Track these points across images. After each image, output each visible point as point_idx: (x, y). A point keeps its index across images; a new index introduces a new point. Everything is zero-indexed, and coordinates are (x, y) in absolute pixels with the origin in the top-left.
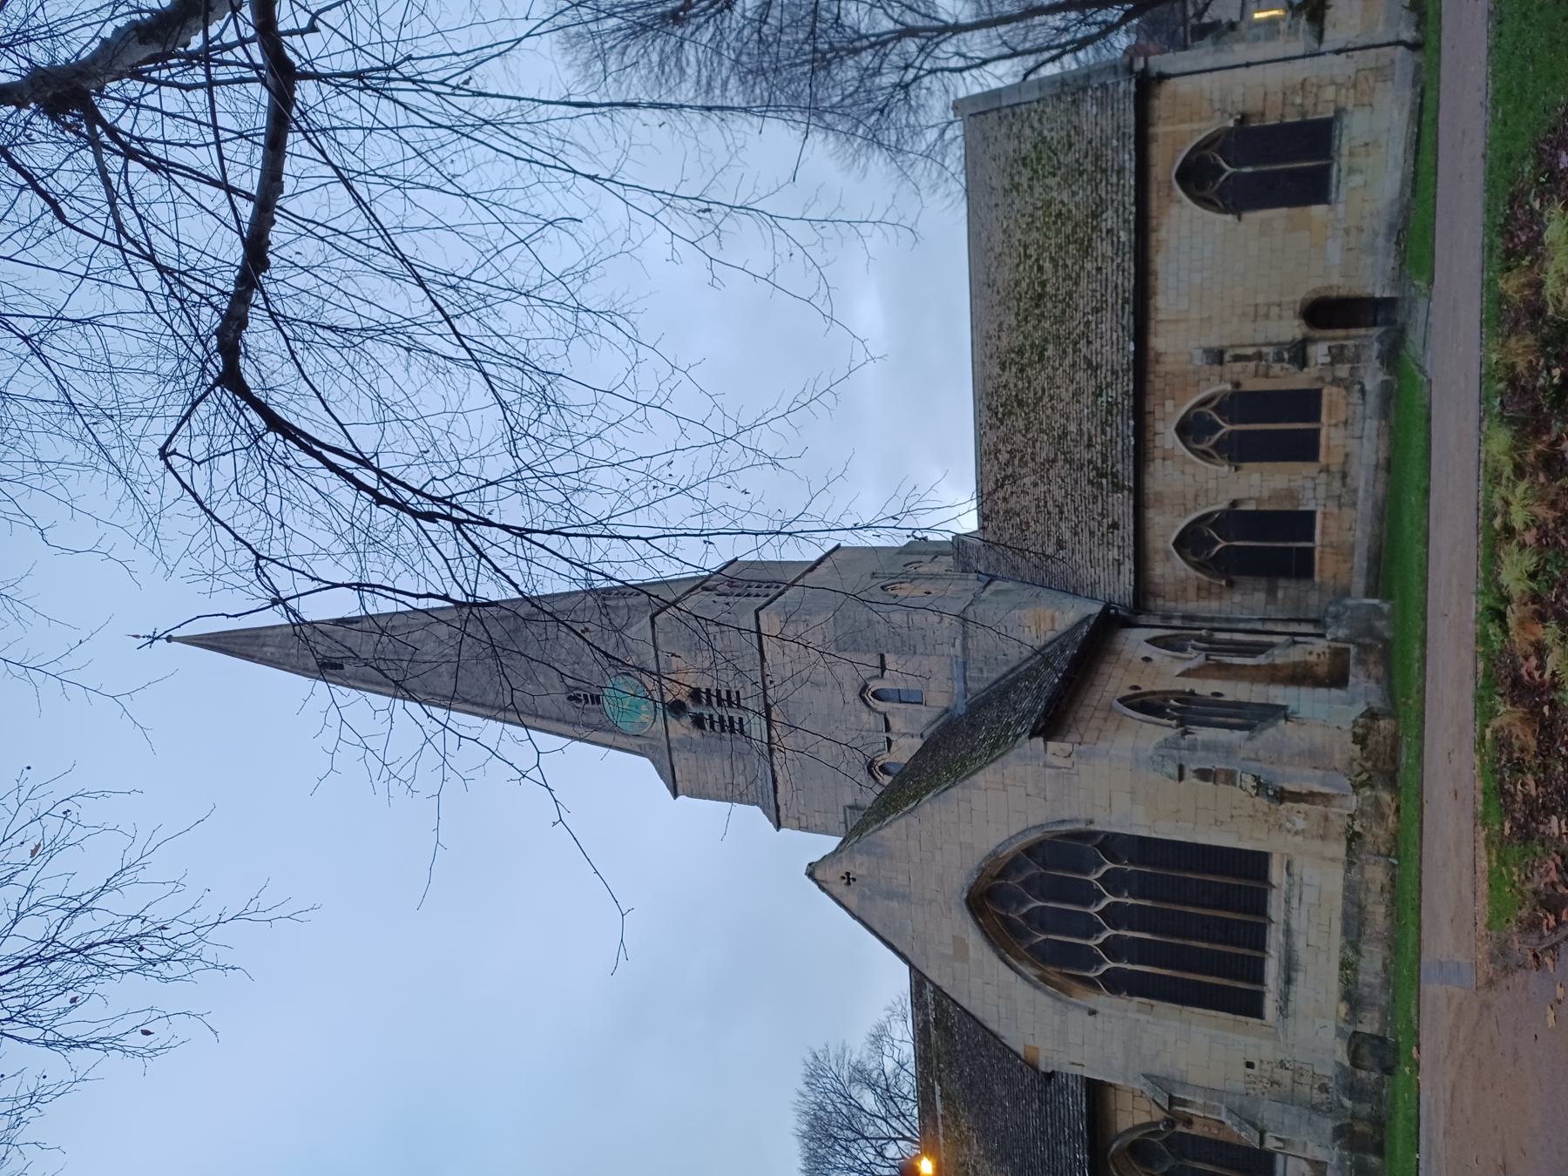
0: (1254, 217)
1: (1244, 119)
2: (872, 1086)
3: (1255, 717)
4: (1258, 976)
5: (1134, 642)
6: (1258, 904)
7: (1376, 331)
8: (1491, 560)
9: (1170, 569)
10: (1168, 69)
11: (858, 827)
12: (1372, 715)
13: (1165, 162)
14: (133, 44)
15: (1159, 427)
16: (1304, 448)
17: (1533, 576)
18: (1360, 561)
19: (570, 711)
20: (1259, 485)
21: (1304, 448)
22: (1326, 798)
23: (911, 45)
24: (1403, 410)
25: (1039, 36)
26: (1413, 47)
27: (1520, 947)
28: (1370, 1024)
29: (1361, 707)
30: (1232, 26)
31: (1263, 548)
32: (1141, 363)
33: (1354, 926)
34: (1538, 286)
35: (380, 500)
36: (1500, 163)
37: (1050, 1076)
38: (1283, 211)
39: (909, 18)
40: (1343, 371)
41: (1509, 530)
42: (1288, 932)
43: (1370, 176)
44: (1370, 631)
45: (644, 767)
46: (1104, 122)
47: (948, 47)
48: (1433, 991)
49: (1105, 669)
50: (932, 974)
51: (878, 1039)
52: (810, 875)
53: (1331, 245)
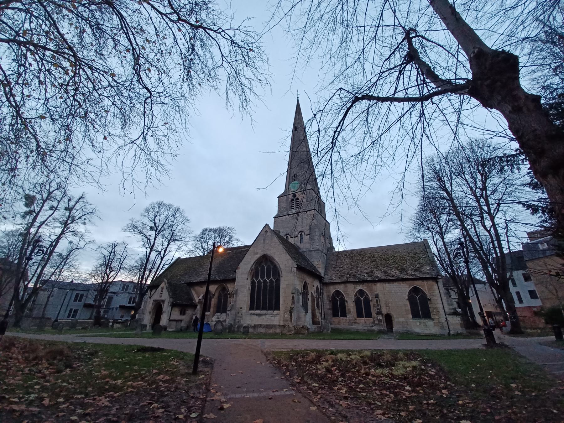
0: (408, 303)
1: (430, 300)
2: (229, 239)
3: (305, 306)
4: (259, 309)
5: (317, 283)
6: (270, 308)
7: (386, 329)
8: (342, 352)
9: (332, 289)
10: (439, 284)
11: (276, 233)
12: (308, 329)
13: (418, 284)
14: (426, 68)
15: (361, 286)
16: (359, 315)
17: (341, 359)
18: (338, 326)
19: (292, 175)
20: (351, 305)
21: (359, 315)
22: (291, 321)
23: (438, 229)
24: (369, 335)
25: (443, 256)
26: (449, 334)
27: (270, 357)
28: (251, 330)
29: (309, 327)
30: (450, 296)
31: (338, 307)
32: (374, 281)
33: (268, 327)
34: (402, 360)
35: (335, 132)
36: (427, 352)
37: (235, 272)
38: (410, 309)
39: (444, 228)
40: (377, 322)
41: (350, 355)
42: (265, 314)
43: (419, 326)
44: (324, 328)
45: (283, 191)
46: (426, 271)
47: (438, 237)
48: (259, 342)
49: (311, 279)
50: (251, 249)
51: (238, 240)
52: (267, 225)
53: (403, 318)
